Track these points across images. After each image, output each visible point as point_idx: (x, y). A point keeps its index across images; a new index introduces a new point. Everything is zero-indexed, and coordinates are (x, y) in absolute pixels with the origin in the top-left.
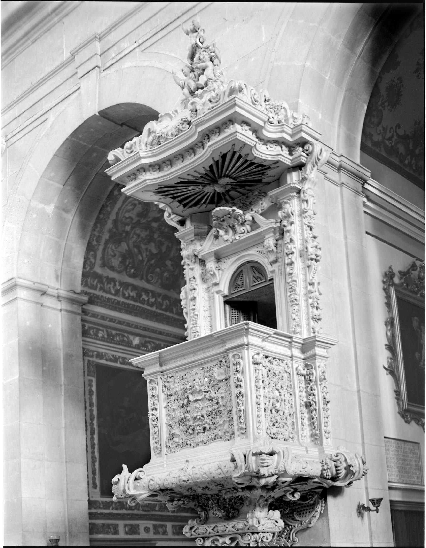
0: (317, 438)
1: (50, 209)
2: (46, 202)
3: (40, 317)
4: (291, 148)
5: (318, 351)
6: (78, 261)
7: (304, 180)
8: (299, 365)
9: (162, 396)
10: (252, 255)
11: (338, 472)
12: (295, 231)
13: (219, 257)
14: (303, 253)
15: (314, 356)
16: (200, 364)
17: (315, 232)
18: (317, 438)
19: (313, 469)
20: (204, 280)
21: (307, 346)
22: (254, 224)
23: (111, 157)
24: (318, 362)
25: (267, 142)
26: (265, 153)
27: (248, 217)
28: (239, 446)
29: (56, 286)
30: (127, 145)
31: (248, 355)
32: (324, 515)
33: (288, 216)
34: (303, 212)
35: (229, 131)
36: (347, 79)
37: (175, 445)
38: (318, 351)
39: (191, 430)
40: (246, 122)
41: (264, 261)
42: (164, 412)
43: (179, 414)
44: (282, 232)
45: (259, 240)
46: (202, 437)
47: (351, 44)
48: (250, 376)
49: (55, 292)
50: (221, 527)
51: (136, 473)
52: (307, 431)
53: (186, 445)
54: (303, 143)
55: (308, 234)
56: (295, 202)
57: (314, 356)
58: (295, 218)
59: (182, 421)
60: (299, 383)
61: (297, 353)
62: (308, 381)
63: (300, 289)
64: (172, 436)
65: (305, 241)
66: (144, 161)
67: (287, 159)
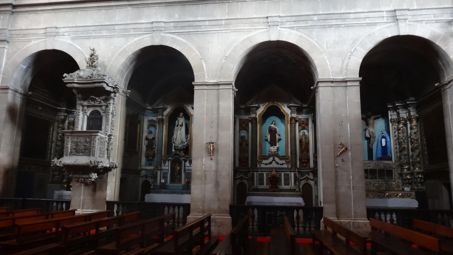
0: (108, 158)
1: (25, 67)
2: (24, 65)
3: (14, 98)
4: (114, 88)
5: (112, 137)
6: (29, 82)
7: (115, 96)
8: (107, 139)
9: (70, 141)
10: (98, 109)
11: (176, 207)
12: (111, 108)
13: (88, 106)
14: (112, 113)
15: (111, 138)
16: (83, 136)
17: (116, 109)
18: (108, 158)
19: (108, 166)
20: (82, 110)
21: (110, 136)
22: (100, 102)
23: (64, 76)
24: (112, 140)
25: (108, 86)
26: (108, 89)
27: (99, 100)
28: (92, 159)
29: (20, 90)
30: (70, 74)
31: (97, 137)
32: (107, 176)
33: (110, 104)
34: (113, 104)
35: (101, 84)
36: (128, 70)
37: (71, 154)
38: (112, 137)
39: (77, 151)
40: (105, 82)
41: (101, 112)
42: (70, 145)
43: (74, 147)
44: (107, 106)
45: (101, 106)
46: (81, 154)
47: (131, 64)
48: (97, 142)
49: (20, 92)
50: (81, 176)
51: (60, 160)
52: (106, 155)
53: (75, 155)
54: (117, 88)
55: (114, 109)
56: (112, 101)
57: (111, 138)
58: (112, 105)
59: (75, 149)
60: (106, 144)
61: (107, 137)
62: (108, 144)
63: (110, 122)
64: (71, 152)
65: (113, 111)
66: (75, 81)
67: (112, 90)
